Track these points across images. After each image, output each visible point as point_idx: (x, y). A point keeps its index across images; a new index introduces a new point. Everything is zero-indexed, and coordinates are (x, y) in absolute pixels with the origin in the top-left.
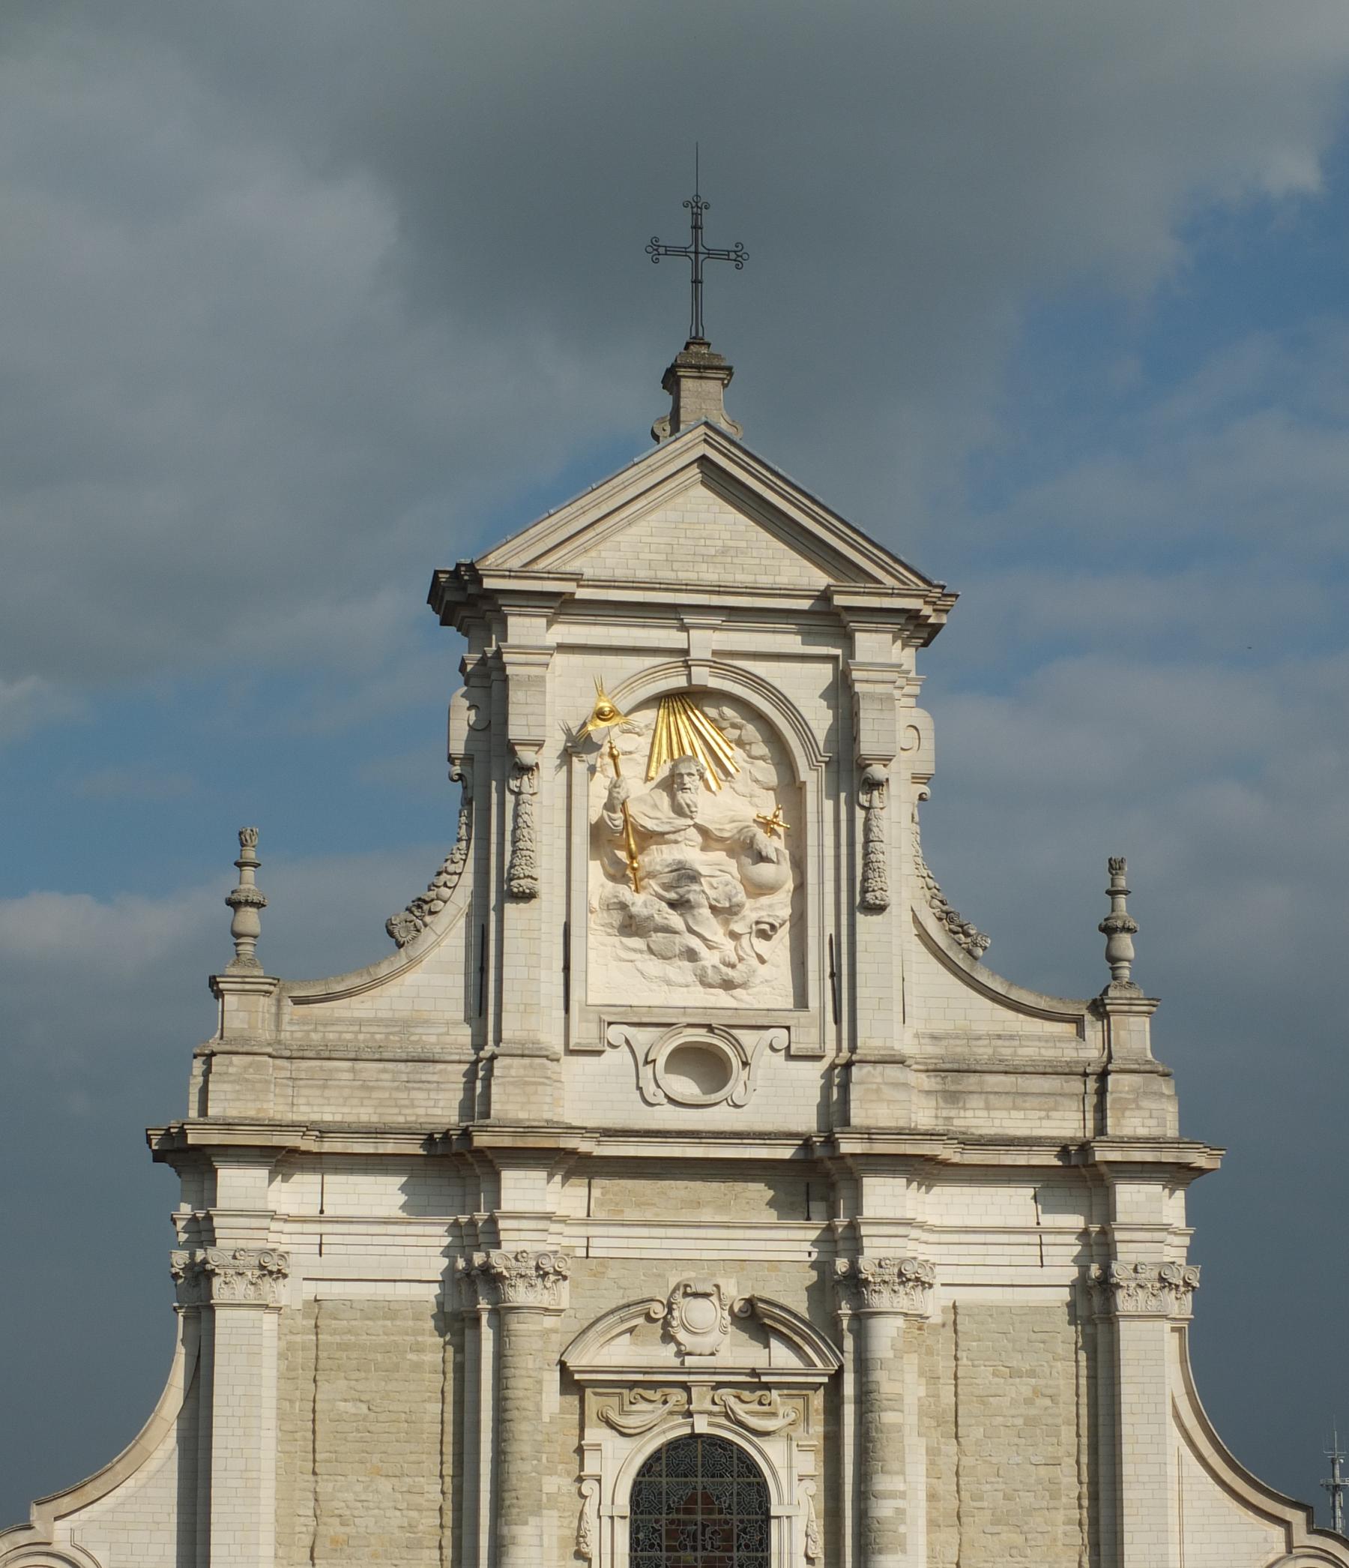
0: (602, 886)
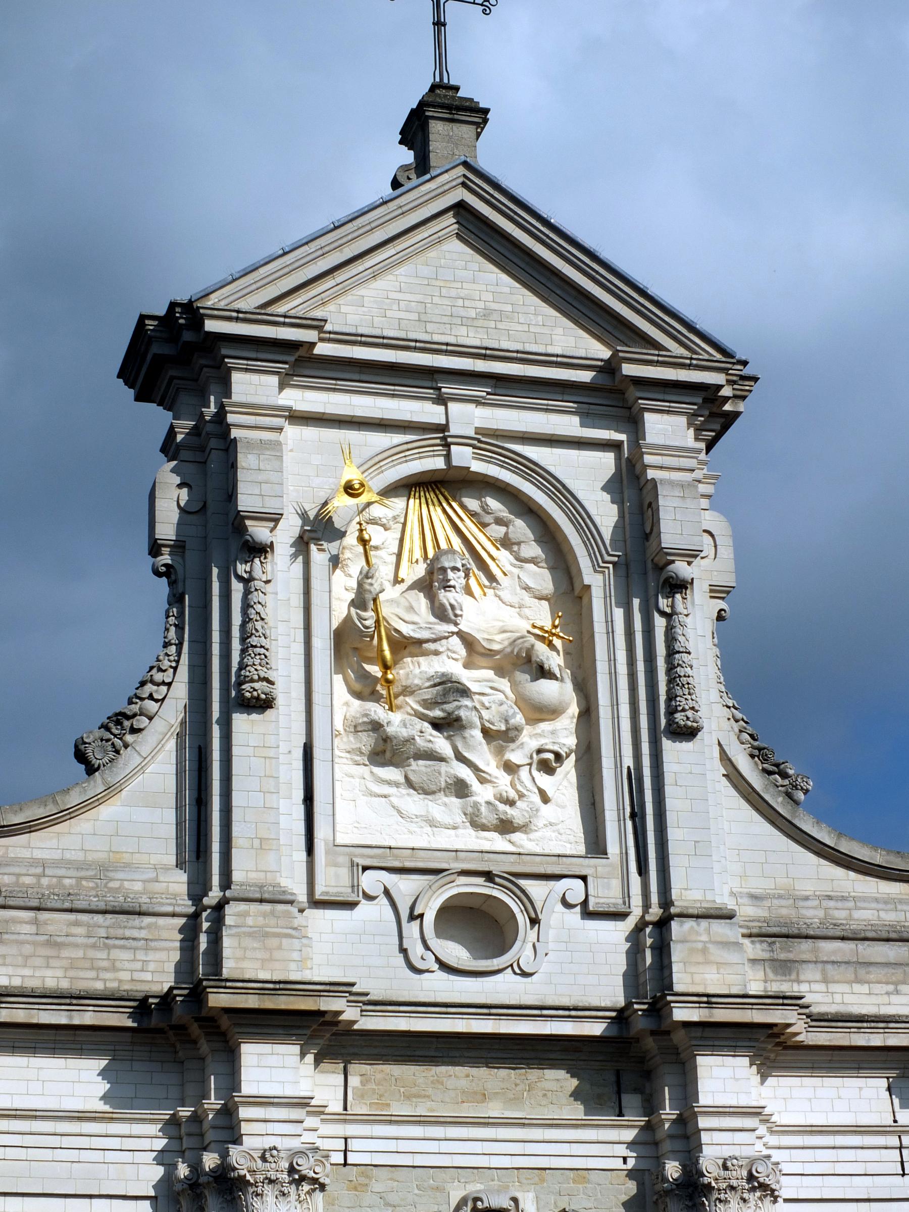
0: (347, 704)
